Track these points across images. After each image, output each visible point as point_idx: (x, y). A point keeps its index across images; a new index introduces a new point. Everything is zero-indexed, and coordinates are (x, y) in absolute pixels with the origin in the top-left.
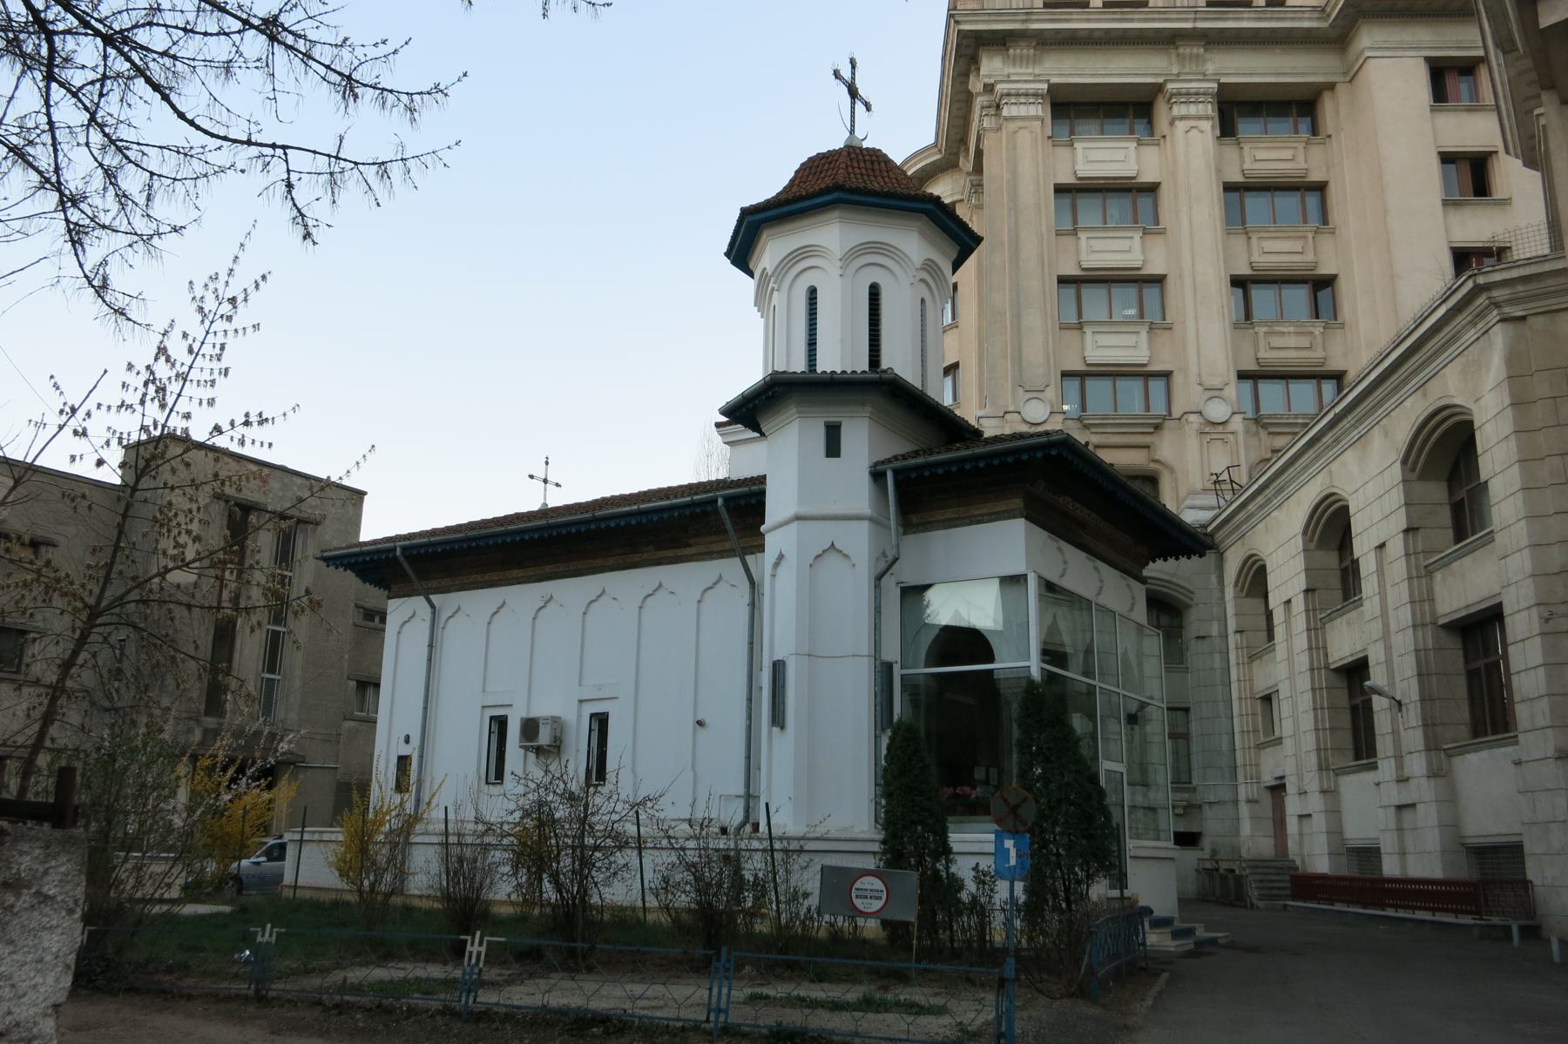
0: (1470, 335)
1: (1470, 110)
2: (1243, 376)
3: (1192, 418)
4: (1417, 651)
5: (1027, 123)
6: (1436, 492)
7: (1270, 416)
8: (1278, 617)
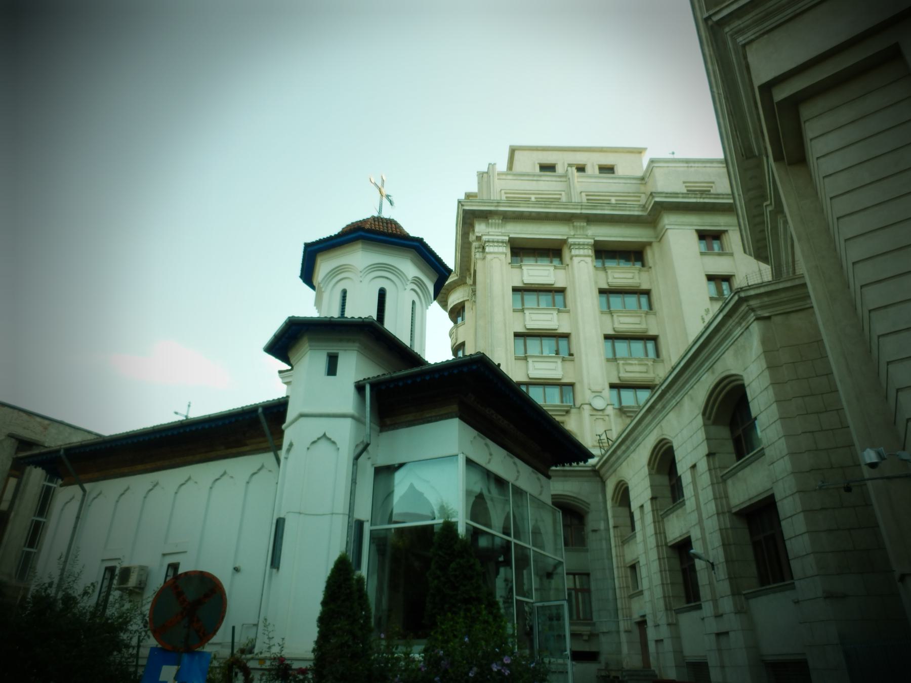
0: (738, 331)
1: (719, 255)
4: (721, 529)
6: (724, 432)
7: (628, 407)
8: (637, 516)
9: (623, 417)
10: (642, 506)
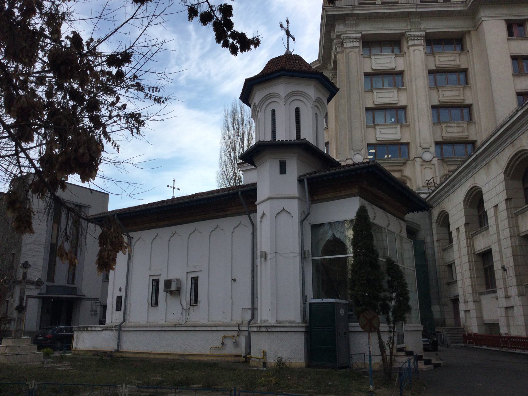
2: (437, 143)
3: (418, 160)
5: (353, 49)
8: (454, 234)
9: (445, 165)
10: (458, 229)
